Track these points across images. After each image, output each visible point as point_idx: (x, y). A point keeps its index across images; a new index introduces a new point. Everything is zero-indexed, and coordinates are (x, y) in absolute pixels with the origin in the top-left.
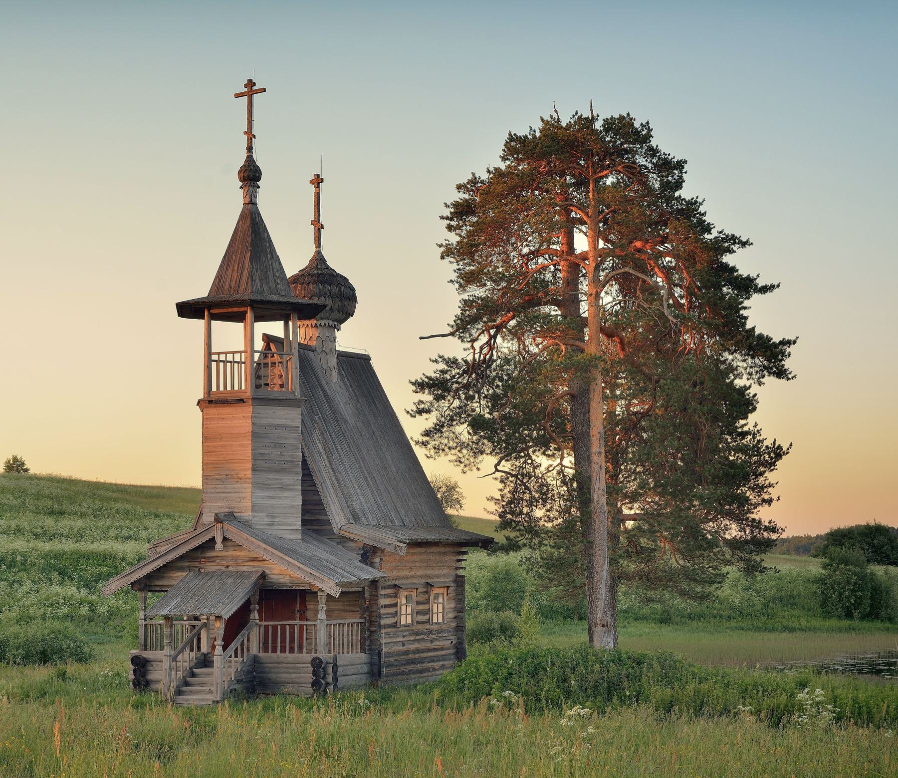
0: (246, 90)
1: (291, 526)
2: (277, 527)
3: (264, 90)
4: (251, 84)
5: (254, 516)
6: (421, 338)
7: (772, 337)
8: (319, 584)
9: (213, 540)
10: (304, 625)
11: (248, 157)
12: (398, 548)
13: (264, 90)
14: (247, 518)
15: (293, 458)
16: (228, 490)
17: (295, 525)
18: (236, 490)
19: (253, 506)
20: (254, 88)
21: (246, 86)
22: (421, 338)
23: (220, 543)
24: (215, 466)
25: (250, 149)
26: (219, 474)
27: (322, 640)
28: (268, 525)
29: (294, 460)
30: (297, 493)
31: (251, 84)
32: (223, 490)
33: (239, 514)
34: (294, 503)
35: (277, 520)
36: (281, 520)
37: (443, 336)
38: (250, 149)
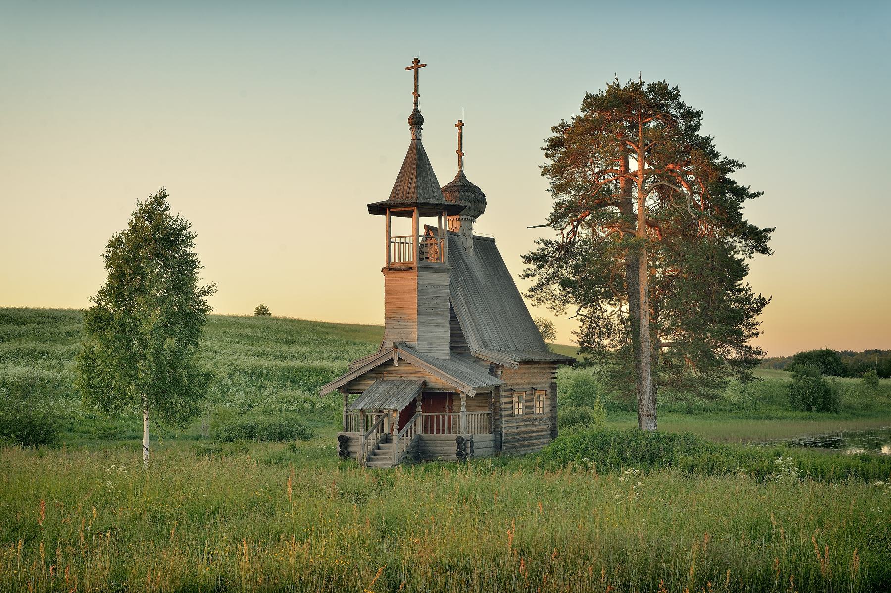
0: (413, 65)
4: (416, 61)
5: (419, 344)
6: (528, 227)
9: (392, 359)
14: (415, 345)
17: (446, 350)
19: (418, 338)
20: (419, 64)
21: (413, 63)
22: (528, 227)
25: (416, 104)
31: (416, 61)
32: (398, 327)
35: (433, 346)
38: (416, 104)
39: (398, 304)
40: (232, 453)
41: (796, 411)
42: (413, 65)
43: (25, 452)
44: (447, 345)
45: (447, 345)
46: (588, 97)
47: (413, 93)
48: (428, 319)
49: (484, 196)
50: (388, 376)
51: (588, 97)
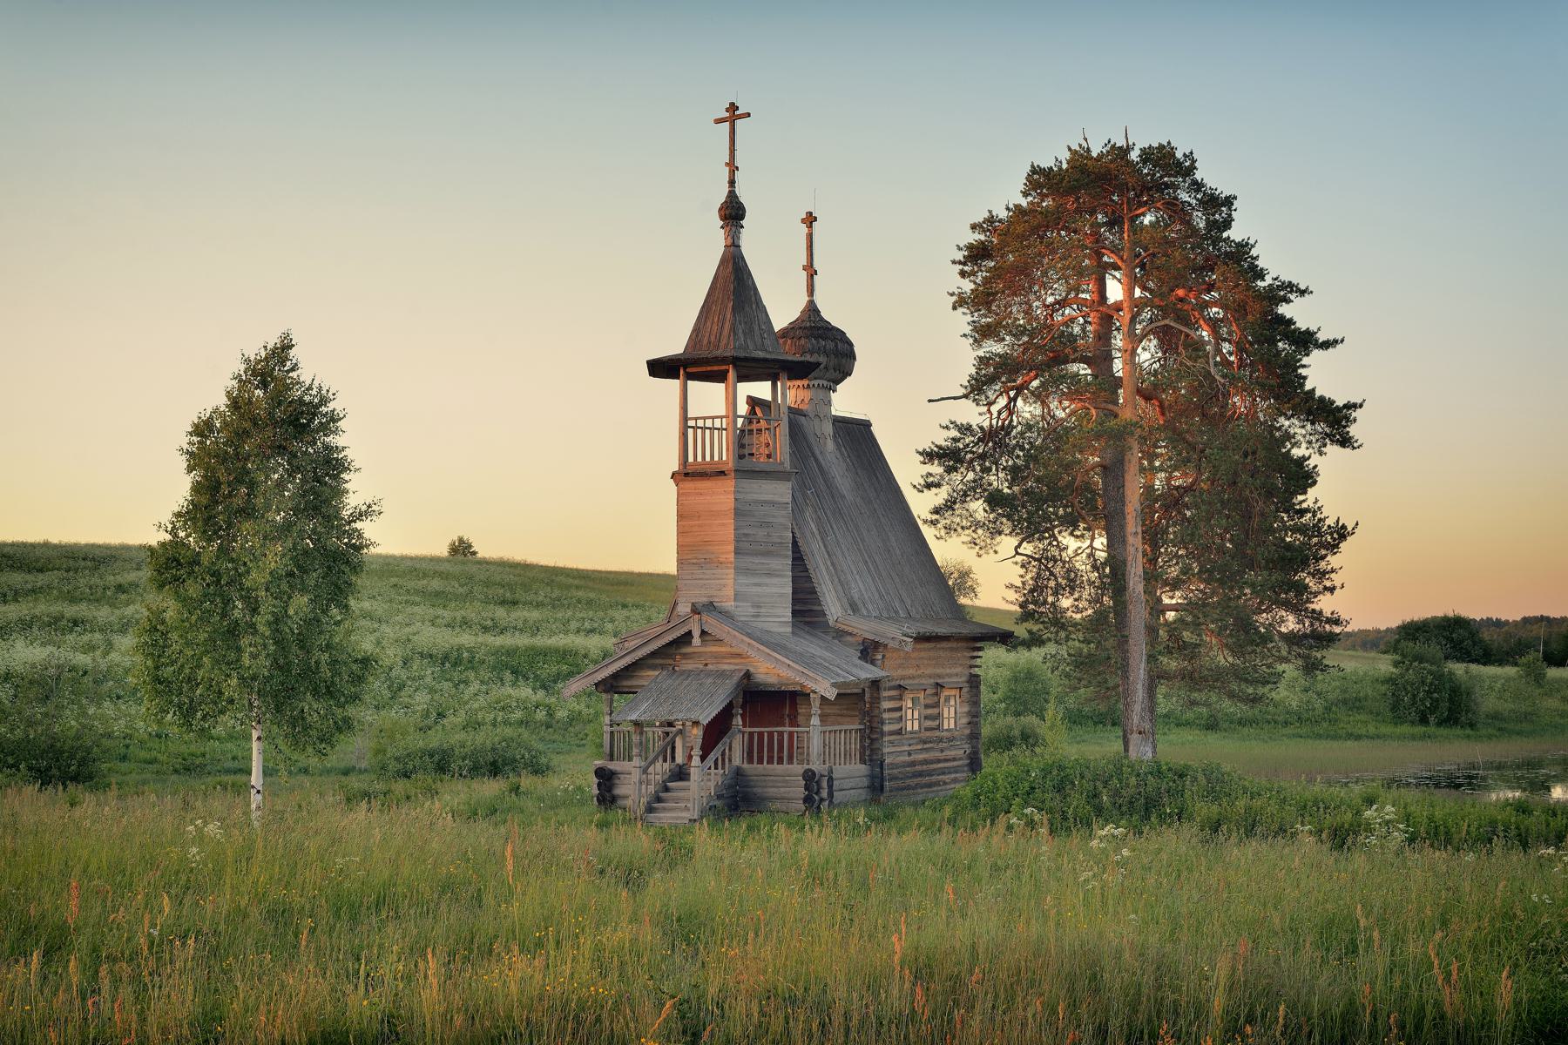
0: (728, 114)
4: (733, 107)
9: (689, 634)
11: (730, 192)
17: (783, 616)
21: (727, 110)
25: (732, 183)
31: (733, 107)
38: (732, 183)
47: (727, 164)
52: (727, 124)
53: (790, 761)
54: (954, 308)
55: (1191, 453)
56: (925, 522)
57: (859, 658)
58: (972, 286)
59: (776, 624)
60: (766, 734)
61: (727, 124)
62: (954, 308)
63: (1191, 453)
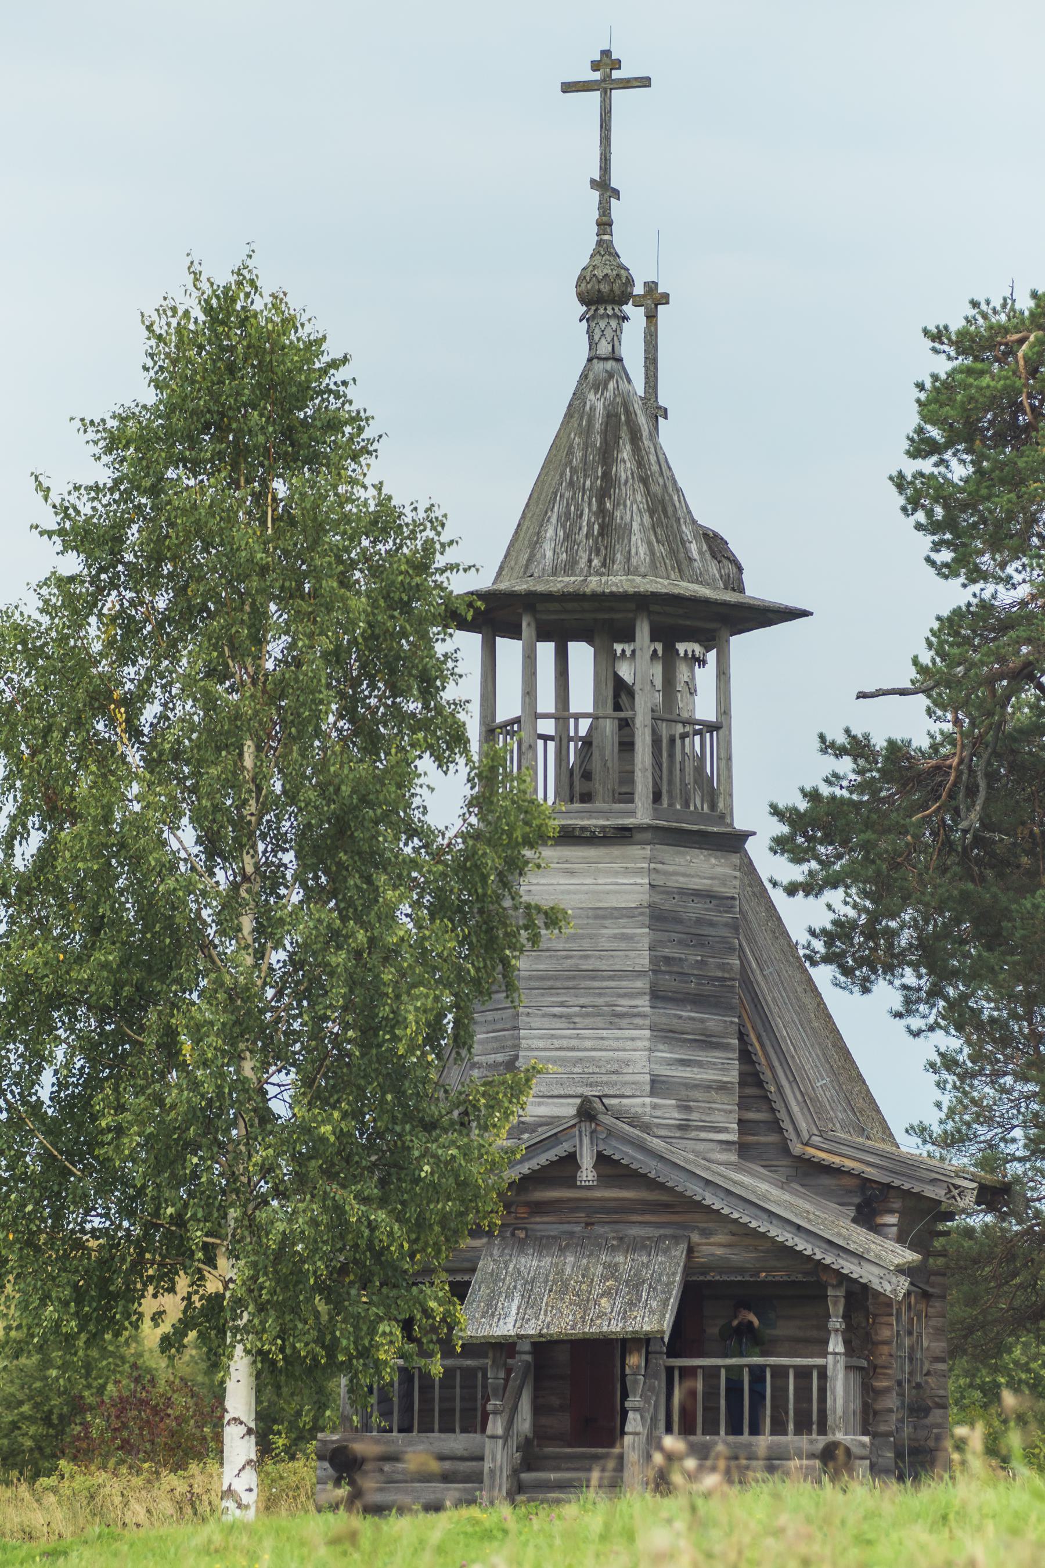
0: (597, 76)
1: (719, 1132)
2: (693, 1134)
3: (645, 82)
4: (607, 62)
5: (655, 1107)
6: (862, 695)
7: (907, 737)
8: (853, 1267)
9: (571, 1160)
10: (765, 1366)
11: (600, 243)
12: (955, 1192)
13: (645, 82)
14: (640, 1110)
15: (724, 970)
16: (588, 1044)
17: (725, 1130)
18: (606, 1043)
19: (653, 1082)
20: (616, 74)
21: (595, 66)
22: (862, 695)
23: (590, 1168)
24: (549, 983)
25: (605, 224)
26: (562, 1005)
27: (840, 1402)
28: (680, 1127)
29: (726, 975)
30: (730, 1055)
31: (607, 62)
32: (573, 1043)
33: (615, 1101)
34: (725, 1079)
35: (695, 1116)
36: (704, 1118)
37: (903, 692)
38: (605, 224)
39: (571, 957)
40: (945, 1518)
41: (149, 1370)
42: (597, 76)
43: (749, 1496)
44: (731, 1112)
45: (731, 1112)
46: (667, 303)
47: (594, 183)
48: (680, 1017)
49: (740, 569)
50: (533, 1220)
51: (667, 303)
52: (597, 95)
53: (755, 1431)
54: (324, 337)
55: (204, 520)
56: (792, 890)
57: (854, 1220)
58: (624, 307)
59: (712, 1145)
60: (723, 1372)
61: (597, 95)
62: (324, 337)
63: (204, 520)
